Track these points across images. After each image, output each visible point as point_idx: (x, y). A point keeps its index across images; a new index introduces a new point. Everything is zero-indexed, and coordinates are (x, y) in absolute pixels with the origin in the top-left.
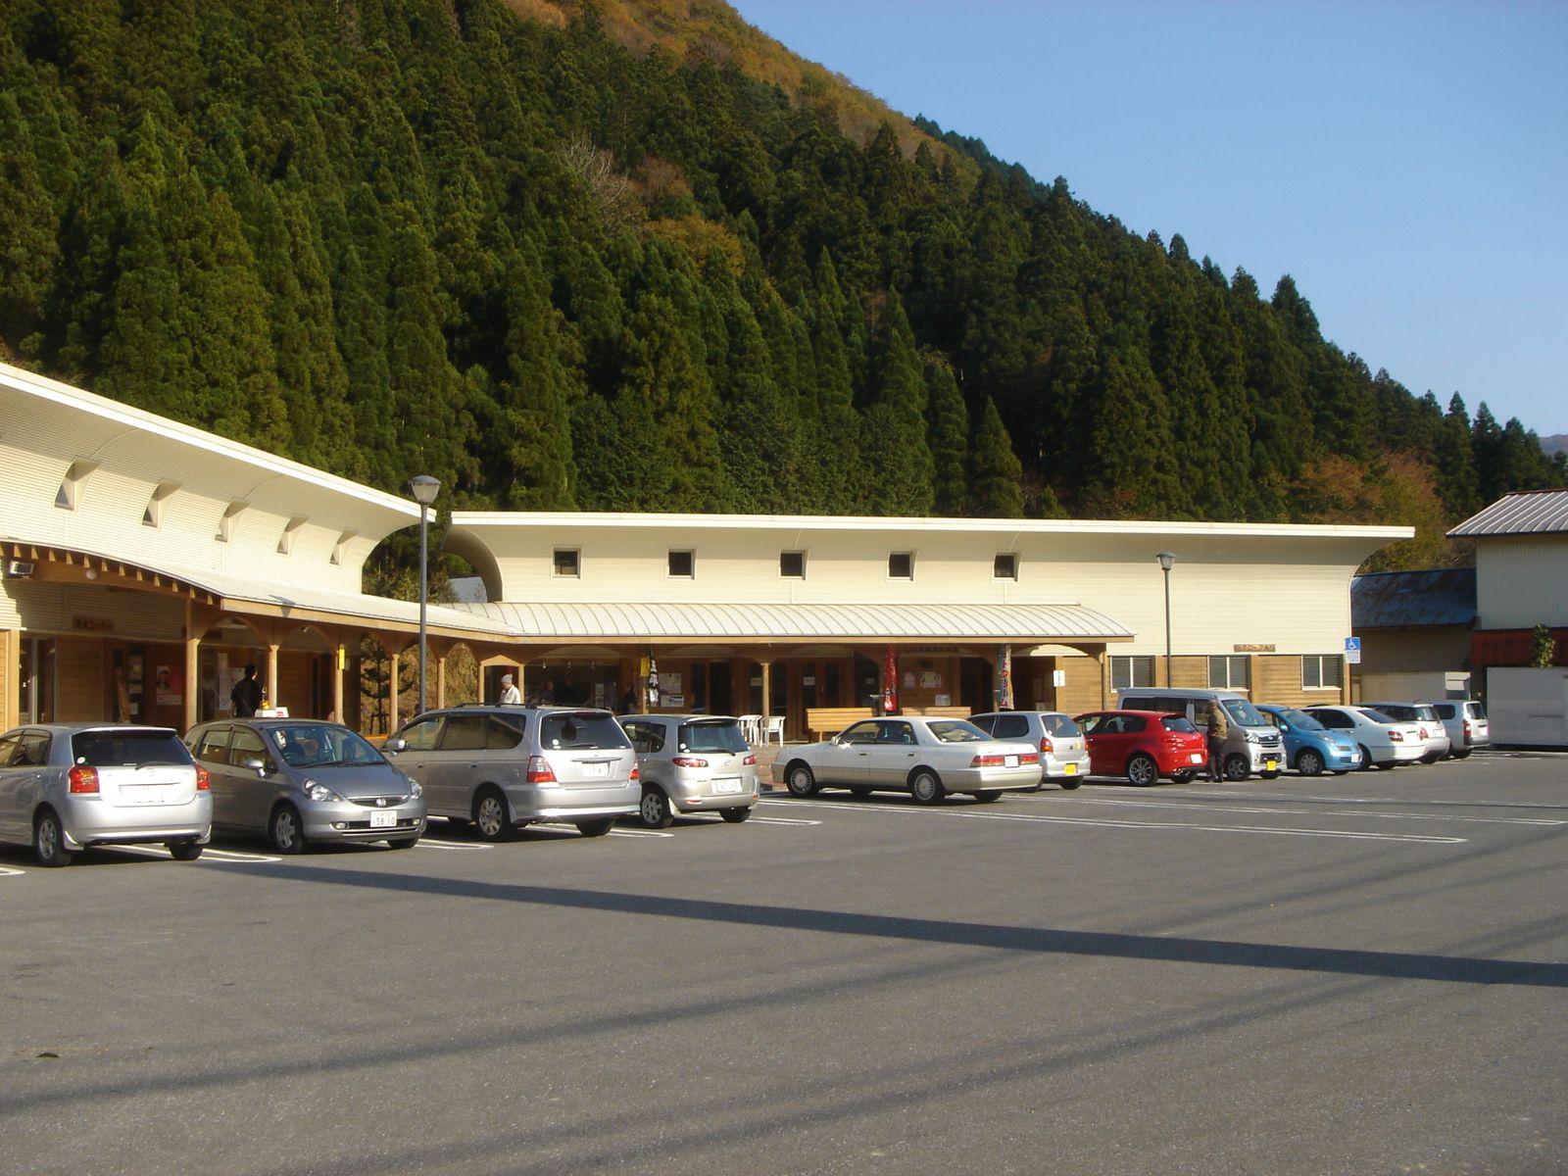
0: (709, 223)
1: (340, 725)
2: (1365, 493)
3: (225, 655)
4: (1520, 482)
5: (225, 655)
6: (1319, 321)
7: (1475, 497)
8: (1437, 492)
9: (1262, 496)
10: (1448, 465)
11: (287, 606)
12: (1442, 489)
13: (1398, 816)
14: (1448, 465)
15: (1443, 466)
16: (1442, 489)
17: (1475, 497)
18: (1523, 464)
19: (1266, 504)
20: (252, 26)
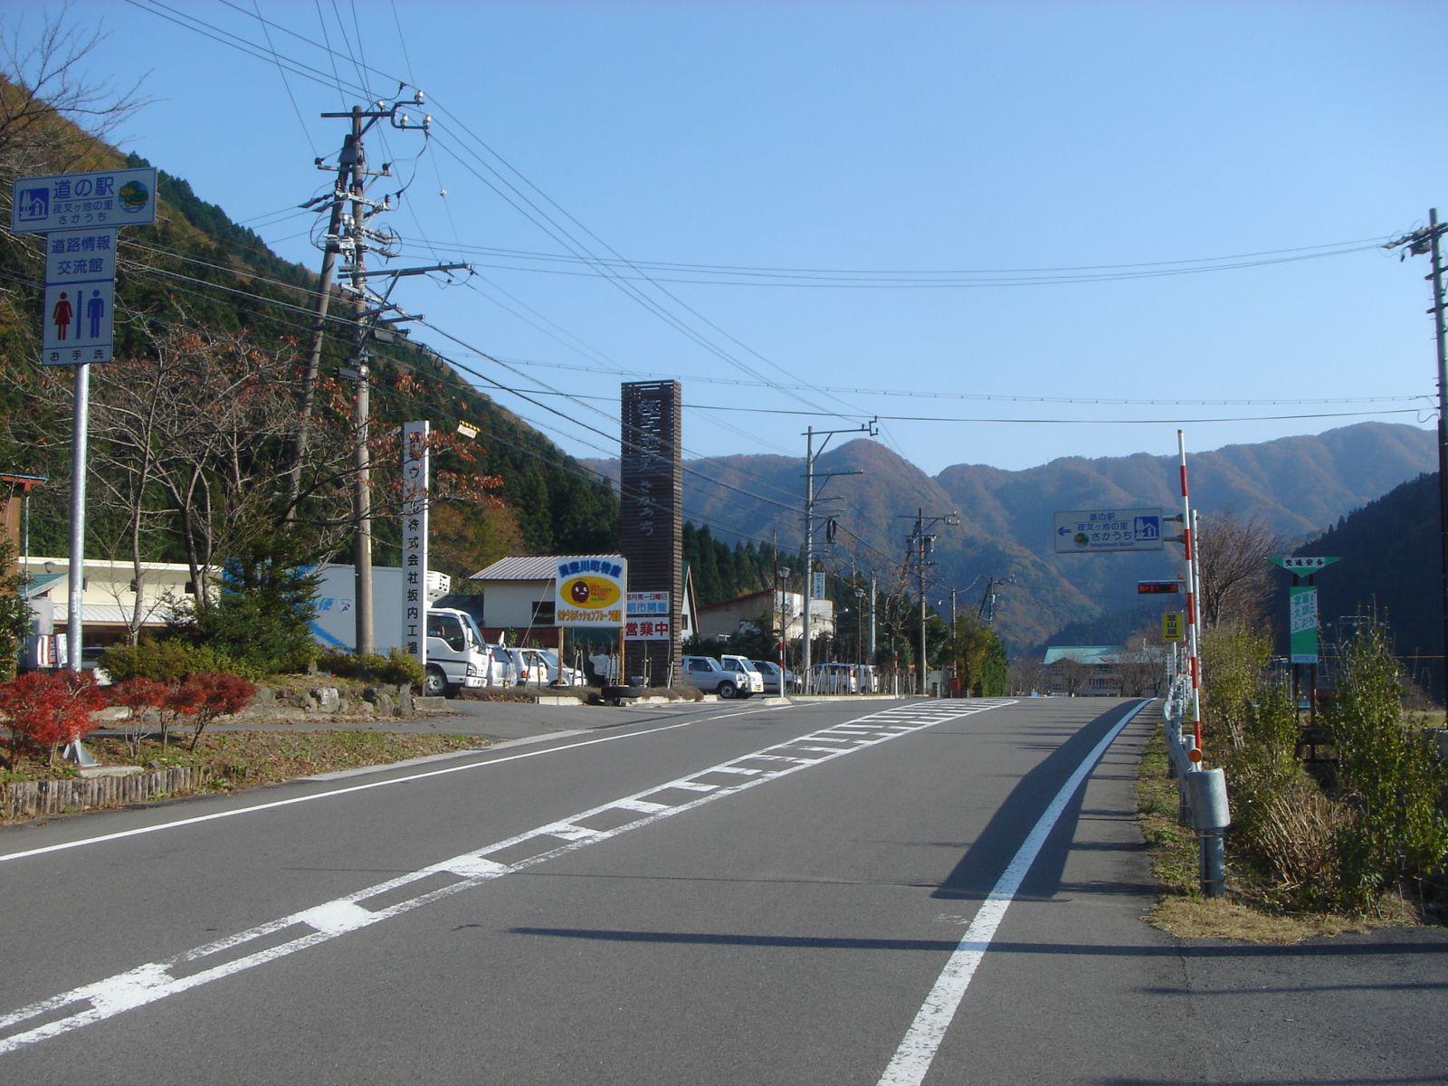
0: (1418, 475)
1: (103, 688)
2: (463, 530)
3: (1312, 594)
4: (580, 522)
5: (1312, 594)
6: (1102, 456)
7: (548, 531)
8: (521, 526)
9: (391, 531)
10: (530, 507)
11: (727, 610)
12: (525, 525)
13: (1198, 608)
14: (530, 507)
15: (526, 508)
16: (525, 525)
17: (548, 531)
18: (582, 510)
19: (394, 536)
20: (1372, 1041)
